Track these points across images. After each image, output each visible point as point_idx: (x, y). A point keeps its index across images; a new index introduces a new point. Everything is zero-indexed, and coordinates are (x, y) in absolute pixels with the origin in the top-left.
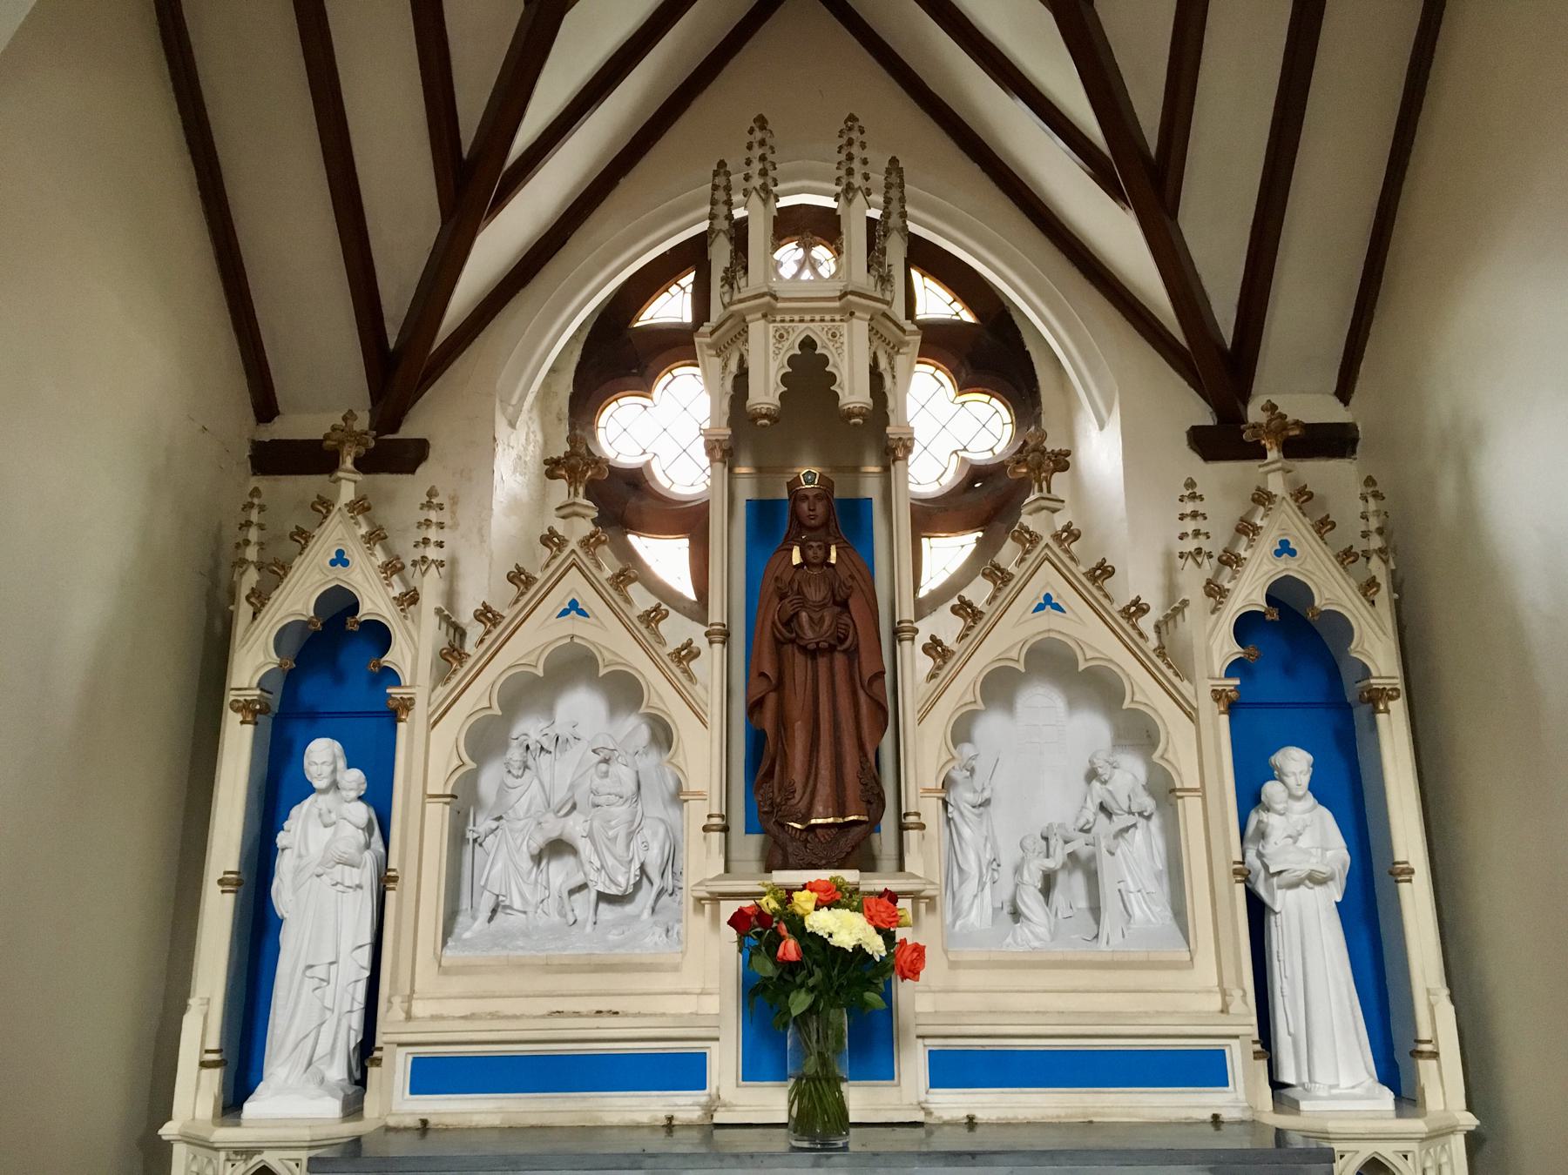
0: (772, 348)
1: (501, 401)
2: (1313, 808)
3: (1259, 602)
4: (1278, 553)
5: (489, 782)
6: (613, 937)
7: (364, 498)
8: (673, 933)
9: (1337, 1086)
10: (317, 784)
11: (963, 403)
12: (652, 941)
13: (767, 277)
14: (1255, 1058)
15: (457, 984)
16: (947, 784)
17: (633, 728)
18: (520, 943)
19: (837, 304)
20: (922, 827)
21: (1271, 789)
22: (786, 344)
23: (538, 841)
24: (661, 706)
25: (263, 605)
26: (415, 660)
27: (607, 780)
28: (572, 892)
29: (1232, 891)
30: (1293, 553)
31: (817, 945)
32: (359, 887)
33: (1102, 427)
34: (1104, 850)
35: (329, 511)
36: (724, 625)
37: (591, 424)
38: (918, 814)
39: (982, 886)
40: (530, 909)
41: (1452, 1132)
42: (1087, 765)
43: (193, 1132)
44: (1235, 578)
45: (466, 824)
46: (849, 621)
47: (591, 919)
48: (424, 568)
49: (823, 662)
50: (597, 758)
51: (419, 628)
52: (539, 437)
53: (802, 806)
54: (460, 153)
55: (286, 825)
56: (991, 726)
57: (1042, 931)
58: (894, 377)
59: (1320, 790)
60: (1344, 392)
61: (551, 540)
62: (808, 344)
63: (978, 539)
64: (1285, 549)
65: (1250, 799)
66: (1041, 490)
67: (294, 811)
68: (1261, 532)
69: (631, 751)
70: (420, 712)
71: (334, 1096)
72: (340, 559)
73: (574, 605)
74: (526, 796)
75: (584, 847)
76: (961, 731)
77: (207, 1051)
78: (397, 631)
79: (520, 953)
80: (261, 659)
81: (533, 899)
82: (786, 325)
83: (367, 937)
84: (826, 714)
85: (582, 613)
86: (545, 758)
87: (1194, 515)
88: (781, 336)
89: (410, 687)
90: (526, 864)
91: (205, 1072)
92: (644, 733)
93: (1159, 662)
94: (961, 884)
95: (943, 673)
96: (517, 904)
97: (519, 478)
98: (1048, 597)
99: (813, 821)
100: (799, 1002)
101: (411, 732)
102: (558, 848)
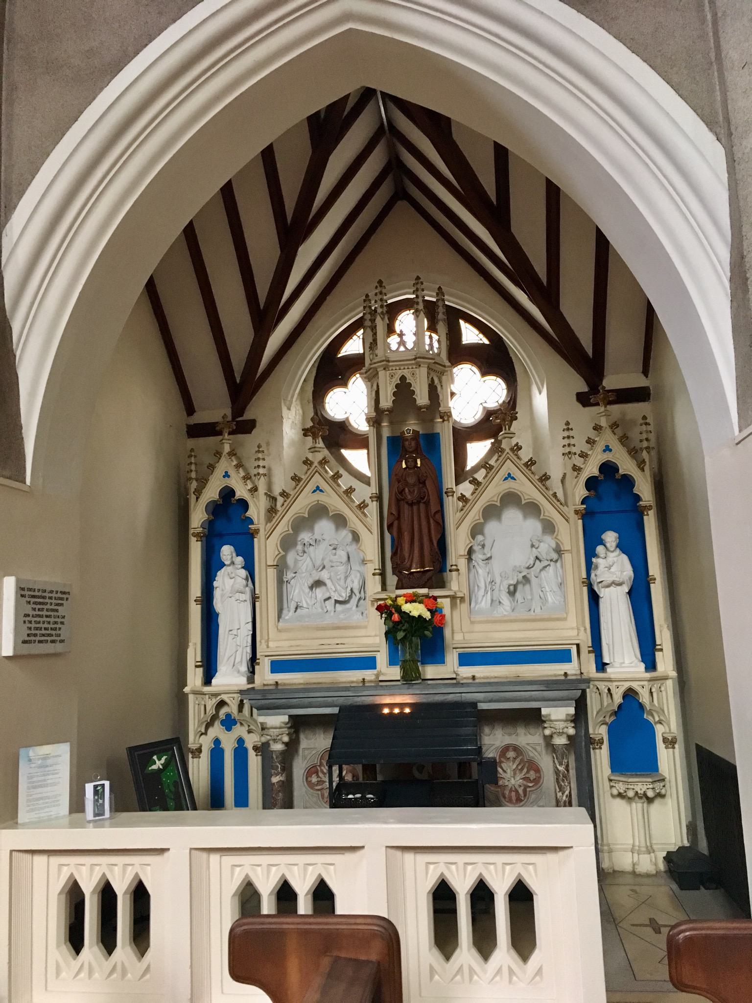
0: (388, 382)
1: (284, 400)
2: (619, 555)
3: (595, 472)
4: (604, 451)
5: (291, 558)
6: (342, 616)
7: (234, 450)
8: (364, 615)
9: (624, 663)
10: (227, 563)
11: (484, 381)
12: (356, 617)
13: (385, 351)
14: (589, 653)
15: (284, 635)
16: (470, 552)
17: (345, 535)
18: (307, 620)
19: (413, 362)
20: (458, 570)
21: (600, 549)
22: (394, 380)
23: (311, 581)
24: (355, 527)
25: (200, 495)
26: (258, 514)
27: (336, 557)
28: (325, 600)
29: (260, 591)
30: (610, 450)
31: (405, 616)
32: (245, 601)
33: (540, 393)
34: (533, 576)
35: (221, 456)
36: (377, 494)
37: (322, 402)
38: (456, 565)
39: (486, 592)
40: (310, 607)
41: (667, 679)
42: (530, 543)
43: (196, 689)
44: (584, 463)
45: (283, 576)
46: (426, 491)
47: (333, 610)
48: (259, 477)
49: (415, 508)
50: (332, 548)
51: (259, 501)
52: (301, 412)
53: (408, 565)
54: (259, 305)
55: (216, 579)
56: (492, 527)
57: (508, 608)
58: (442, 386)
59: (622, 546)
60: (645, 372)
61: (307, 462)
62: (403, 378)
63: (492, 443)
64: (607, 449)
65: (590, 554)
66: (505, 429)
67: (219, 573)
68: (596, 443)
69: (345, 544)
70: (262, 533)
71: (243, 676)
72: (227, 475)
73: (318, 488)
74: (305, 564)
75: (328, 582)
76: (476, 531)
77: (197, 662)
78: (251, 504)
79: (307, 623)
80: (201, 516)
81: (311, 603)
82: (394, 371)
83: (250, 619)
84: (417, 526)
85: (321, 491)
86: (311, 548)
87: (568, 437)
88: (392, 376)
89: (258, 524)
90: (307, 590)
91: (197, 669)
92: (350, 536)
93: (554, 499)
94: (478, 591)
95: (465, 509)
96: (305, 605)
97: (293, 431)
98: (509, 474)
99: (412, 571)
100: (400, 635)
101: (259, 541)
102: (318, 583)
